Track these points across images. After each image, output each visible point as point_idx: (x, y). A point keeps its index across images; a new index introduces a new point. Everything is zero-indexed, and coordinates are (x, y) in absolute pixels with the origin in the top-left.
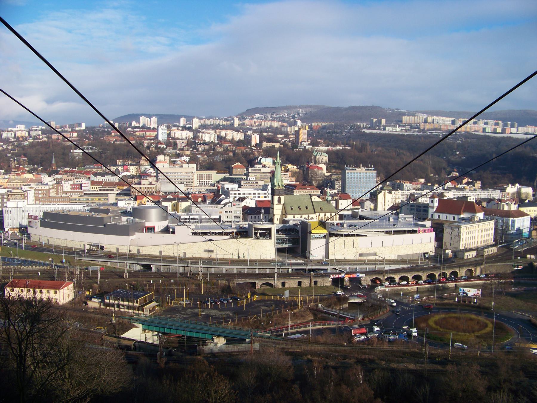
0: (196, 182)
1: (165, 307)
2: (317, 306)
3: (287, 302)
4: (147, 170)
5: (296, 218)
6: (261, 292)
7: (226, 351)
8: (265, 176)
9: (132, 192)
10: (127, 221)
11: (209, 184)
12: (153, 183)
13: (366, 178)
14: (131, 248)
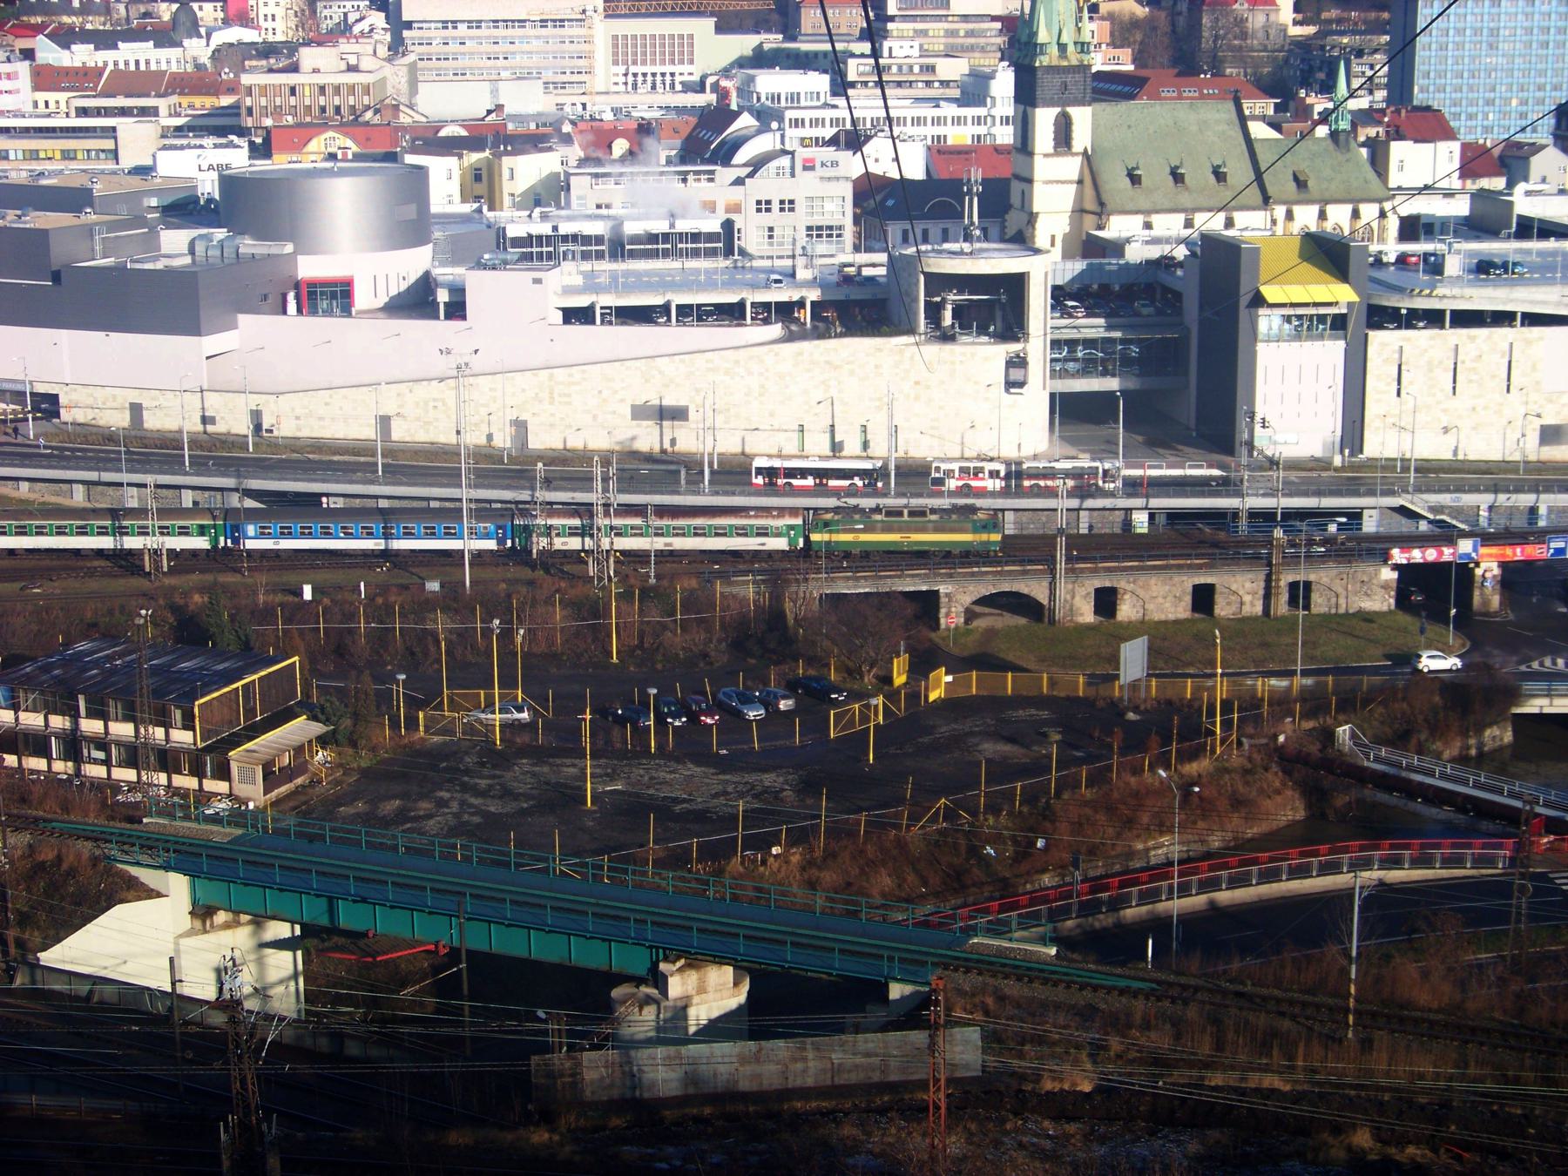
0: (605, 73)
1: (374, 749)
2: (1328, 736)
3: (1136, 709)
4: (352, 18)
5: (1157, 232)
6: (970, 646)
7: (744, 1085)
8: (970, 34)
9: (250, 111)
10: (192, 251)
11: (678, 87)
12: (367, 63)
13: (1529, 31)
14: (214, 404)
